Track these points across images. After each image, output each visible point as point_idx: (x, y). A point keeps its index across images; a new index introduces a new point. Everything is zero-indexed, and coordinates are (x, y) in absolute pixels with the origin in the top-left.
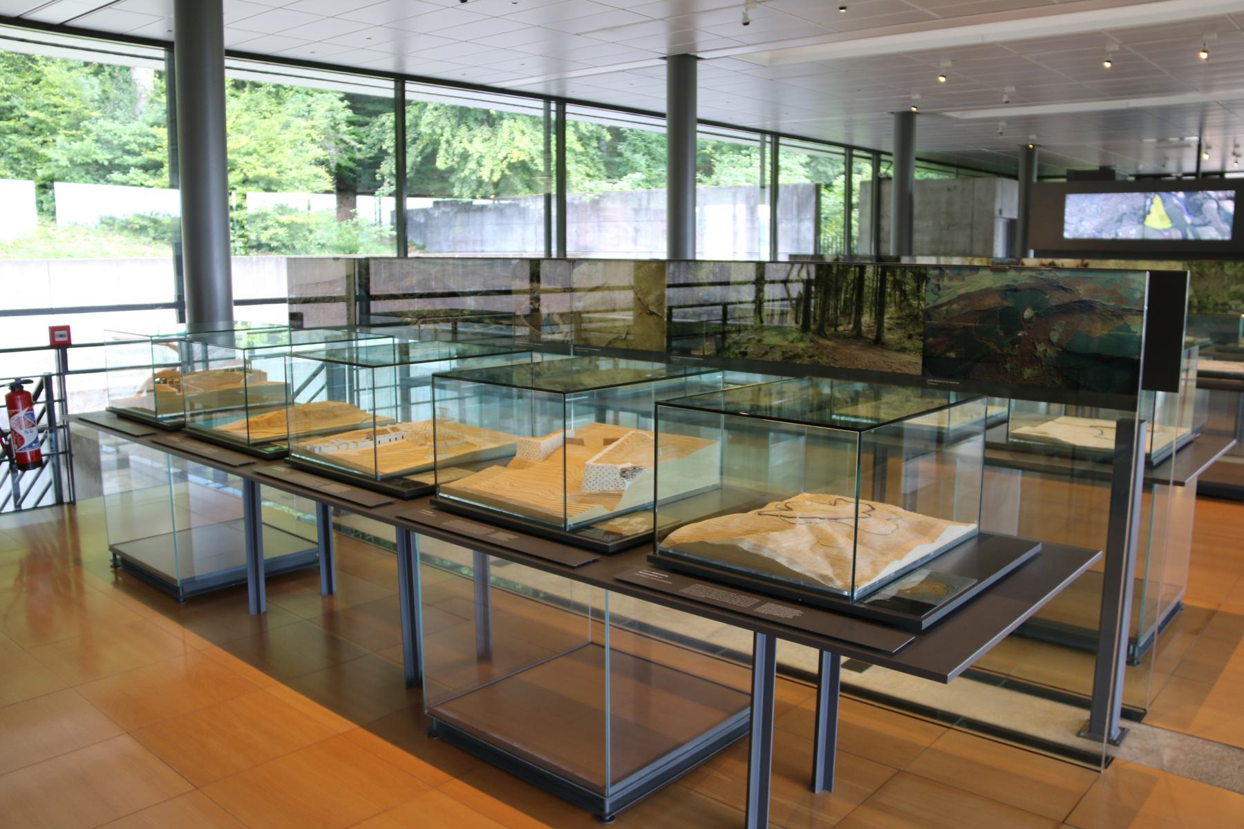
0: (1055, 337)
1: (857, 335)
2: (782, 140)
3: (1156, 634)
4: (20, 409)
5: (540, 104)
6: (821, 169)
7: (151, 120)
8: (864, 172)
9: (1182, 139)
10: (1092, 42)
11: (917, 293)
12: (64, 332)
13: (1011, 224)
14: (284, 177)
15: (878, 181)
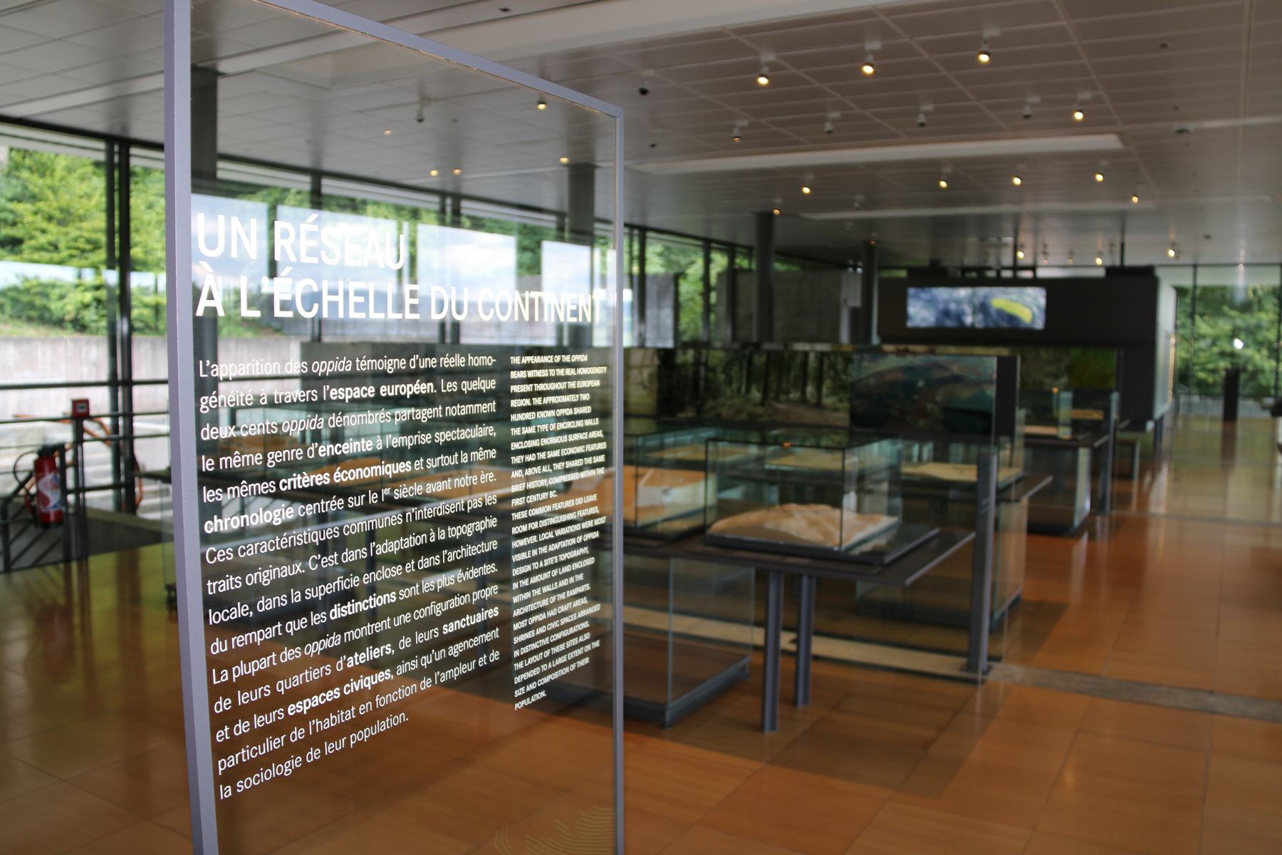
0: (938, 398)
1: (803, 401)
2: (650, 234)
3: (1006, 616)
4: (47, 473)
5: (436, 199)
6: (674, 258)
7: (9, 194)
8: (720, 261)
9: (999, 239)
10: (932, 168)
11: (845, 371)
12: (84, 404)
13: (854, 313)
14: (150, 258)
15: (732, 273)
